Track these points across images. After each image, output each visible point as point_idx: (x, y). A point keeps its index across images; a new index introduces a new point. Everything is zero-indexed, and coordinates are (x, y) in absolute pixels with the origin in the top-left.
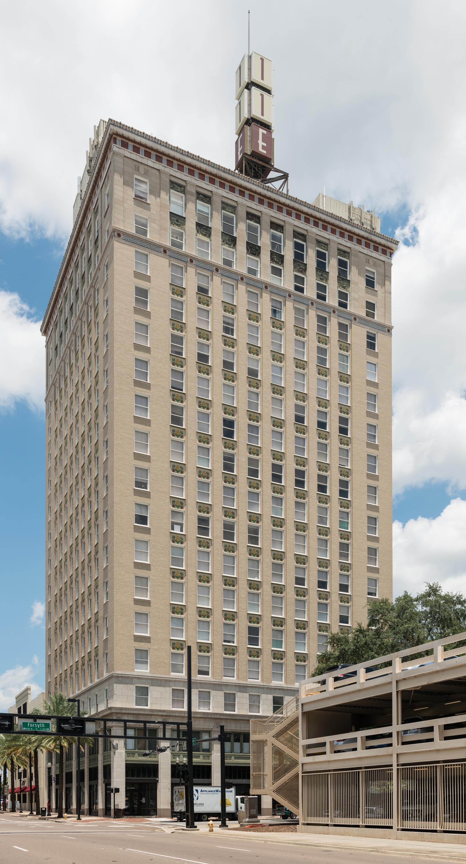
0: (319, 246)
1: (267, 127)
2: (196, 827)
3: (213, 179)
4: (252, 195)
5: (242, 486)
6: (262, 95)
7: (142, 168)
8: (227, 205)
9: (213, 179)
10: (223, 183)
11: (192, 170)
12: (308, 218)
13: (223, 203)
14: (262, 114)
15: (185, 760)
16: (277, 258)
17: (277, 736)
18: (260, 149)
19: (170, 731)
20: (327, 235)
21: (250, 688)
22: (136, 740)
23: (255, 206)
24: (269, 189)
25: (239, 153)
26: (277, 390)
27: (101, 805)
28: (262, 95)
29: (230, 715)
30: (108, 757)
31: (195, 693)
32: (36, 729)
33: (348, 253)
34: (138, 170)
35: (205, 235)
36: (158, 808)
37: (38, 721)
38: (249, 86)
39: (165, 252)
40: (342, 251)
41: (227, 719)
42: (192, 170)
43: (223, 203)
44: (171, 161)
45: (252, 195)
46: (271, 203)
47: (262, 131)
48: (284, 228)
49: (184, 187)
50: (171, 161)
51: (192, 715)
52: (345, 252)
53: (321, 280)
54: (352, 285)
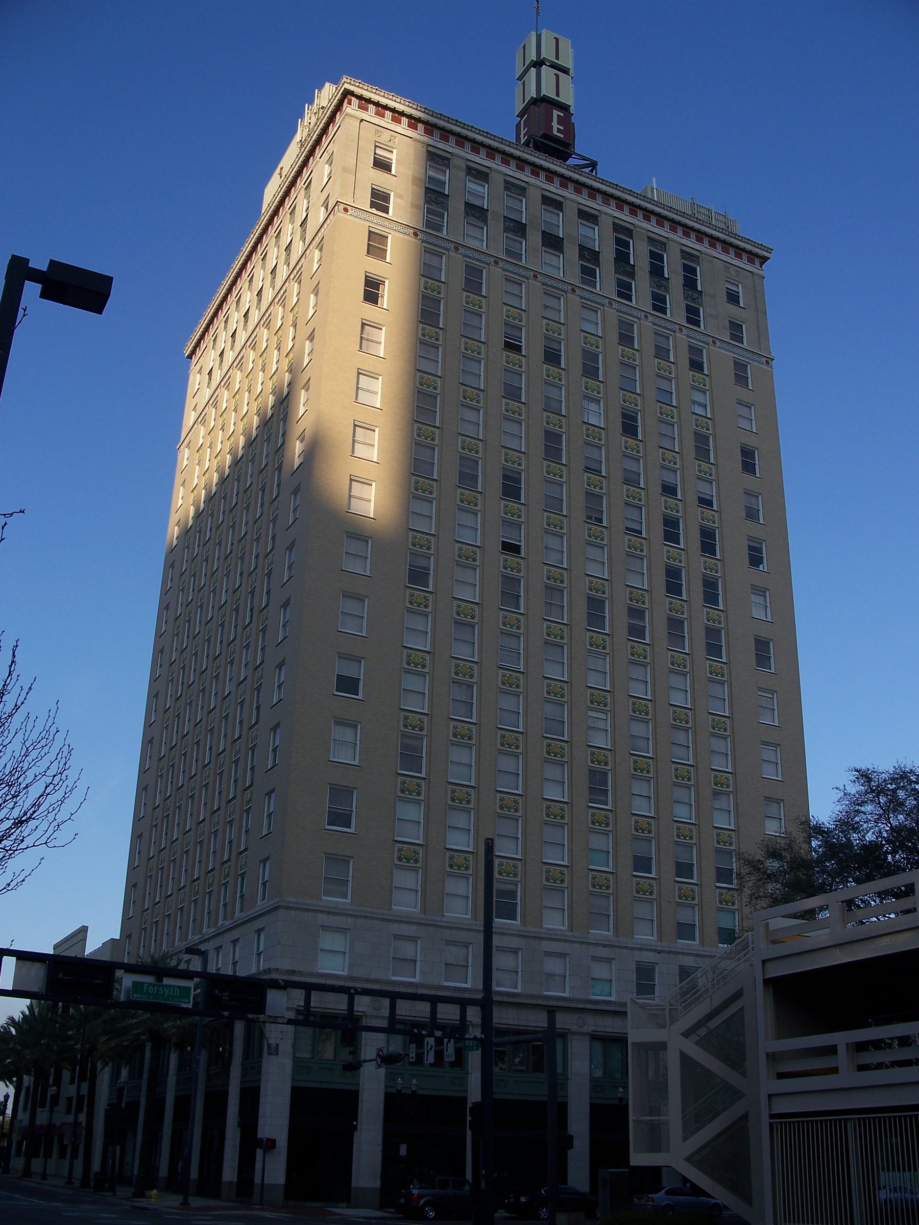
0: (652, 245)
1: (564, 108)
3: (492, 152)
4: (551, 175)
6: (557, 76)
9: (492, 152)
10: (507, 158)
11: (461, 140)
12: (634, 209)
14: (558, 95)
17: (686, 1034)
18: (555, 132)
20: (664, 232)
23: (554, 189)
25: (522, 136)
26: (593, 431)
27: (230, 1173)
28: (557, 76)
30: (253, 1067)
33: (698, 257)
35: (478, 218)
36: (353, 1185)
37: (167, 981)
38: (538, 64)
40: (688, 253)
42: (461, 140)
43: (505, 181)
45: (551, 175)
47: (556, 113)
48: (599, 219)
52: (692, 255)
53: (659, 287)
54: (705, 299)
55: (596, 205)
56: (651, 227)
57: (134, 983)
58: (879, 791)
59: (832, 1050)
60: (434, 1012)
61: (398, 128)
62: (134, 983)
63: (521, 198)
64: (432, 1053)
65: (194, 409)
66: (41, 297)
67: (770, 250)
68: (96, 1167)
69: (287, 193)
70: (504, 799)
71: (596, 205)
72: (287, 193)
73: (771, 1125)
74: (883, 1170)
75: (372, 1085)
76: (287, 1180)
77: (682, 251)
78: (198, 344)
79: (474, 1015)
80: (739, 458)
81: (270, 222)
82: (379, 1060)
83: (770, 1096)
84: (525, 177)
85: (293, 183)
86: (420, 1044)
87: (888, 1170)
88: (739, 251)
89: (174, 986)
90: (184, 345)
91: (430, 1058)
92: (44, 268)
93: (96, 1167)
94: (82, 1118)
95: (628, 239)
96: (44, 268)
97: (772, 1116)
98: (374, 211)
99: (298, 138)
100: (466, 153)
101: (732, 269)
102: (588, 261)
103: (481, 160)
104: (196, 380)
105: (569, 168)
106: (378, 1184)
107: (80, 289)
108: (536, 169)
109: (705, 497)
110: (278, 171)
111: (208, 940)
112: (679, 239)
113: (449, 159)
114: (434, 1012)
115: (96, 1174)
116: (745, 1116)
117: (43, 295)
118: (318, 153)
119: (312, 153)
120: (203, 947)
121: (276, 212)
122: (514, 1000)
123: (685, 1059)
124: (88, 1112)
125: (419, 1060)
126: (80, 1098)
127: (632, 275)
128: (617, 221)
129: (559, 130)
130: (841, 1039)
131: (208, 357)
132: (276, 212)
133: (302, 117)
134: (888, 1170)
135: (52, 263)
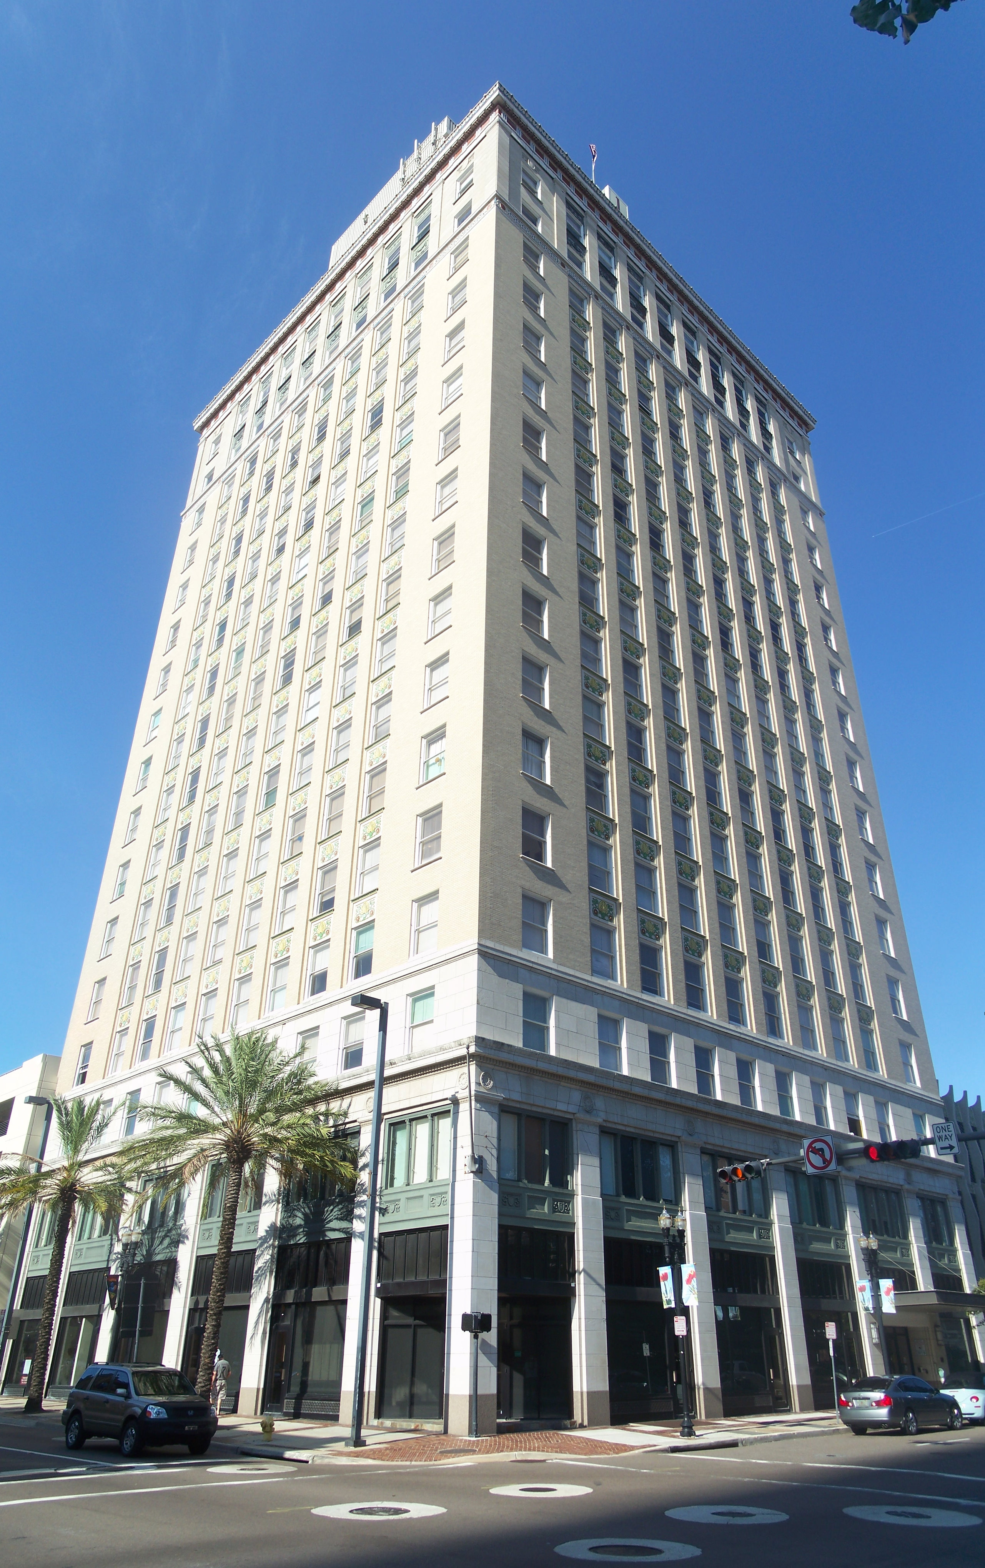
72: (361, 253)
106: (809, 1382)
110: (362, 216)
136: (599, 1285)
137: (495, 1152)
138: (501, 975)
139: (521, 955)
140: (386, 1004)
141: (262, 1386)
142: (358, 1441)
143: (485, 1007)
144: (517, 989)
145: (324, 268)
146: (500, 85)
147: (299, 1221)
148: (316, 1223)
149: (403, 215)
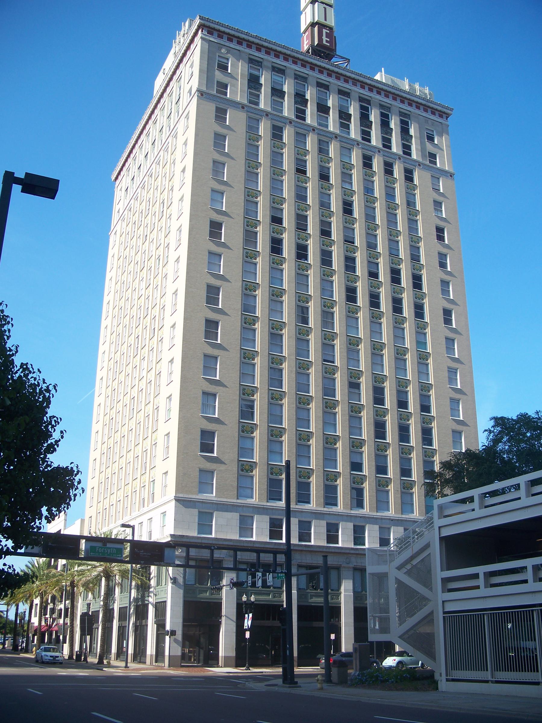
1: (331, 29)
2: (297, 683)
4: (321, 70)
5: (363, 317)
6: (325, 9)
7: (430, 121)
8: (300, 76)
11: (268, 51)
13: (295, 74)
15: (321, 600)
16: (344, 116)
17: (399, 568)
18: (324, 42)
19: (296, 567)
20: (389, 101)
21: (328, 516)
22: (198, 570)
23: (324, 78)
24: (332, 65)
28: (325, 9)
29: (306, 545)
31: (294, 522)
32: (106, 554)
33: (409, 115)
34: (428, 123)
39: (243, 108)
41: (301, 551)
42: (268, 51)
44: (250, 45)
45: (321, 70)
46: (338, 76)
49: (261, 62)
50: (250, 45)
51: (292, 548)
52: (406, 114)
53: (386, 134)
55: (348, 86)
56: (381, 98)
57: (91, 546)
58: (512, 429)
59: (476, 576)
60: (258, 557)
61: (232, 45)
62: (91, 546)
63: (304, 83)
64: (260, 581)
65: (118, 212)
66: (22, 192)
67: (452, 110)
68: (77, 648)
69: (168, 85)
70: (301, 434)
71: (348, 86)
72: (168, 85)
73: (444, 617)
74: (523, 641)
75: (228, 598)
76: (237, 653)
77: (400, 112)
78: (119, 174)
79: (281, 558)
80: (435, 233)
81: (158, 101)
82: (231, 585)
83: (443, 602)
84: (307, 71)
85: (171, 79)
86: (254, 576)
87: (526, 641)
88: (434, 111)
89: (113, 548)
90: (111, 174)
91: (259, 583)
92: (22, 176)
93: (77, 648)
94: (68, 621)
95: (368, 106)
96: (22, 176)
97: (445, 613)
98: (219, 95)
99: (172, 51)
100: (271, 59)
101: (430, 121)
102: (345, 120)
103: (280, 62)
104: (119, 194)
105: (332, 65)
106: (234, 654)
107: (43, 187)
108: (313, 67)
109: (374, 293)
110: (162, 71)
111: (135, 518)
112: (398, 105)
113: (261, 62)
114: (258, 557)
115: (77, 652)
116: (432, 612)
117: (23, 191)
118: (185, 60)
119: (181, 61)
120: (131, 524)
121: (162, 96)
122: (309, 549)
123: (399, 582)
124: (70, 617)
125: (254, 584)
126: (66, 610)
127: (370, 127)
128: (361, 95)
129: (327, 41)
130: (481, 570)
131: (124, 181)
132: (162, 96)
133: (175, 39)
134: (526, 641)
135: (27, 174)
136: (232, 620)
137: (182, 575)
138: (186, 507)
139: (197, 497)
140: (134, 526)
141: (154, 653)
142: (126, 666)
143: (177, 522)
144: (195, 512)
145: (151, 96)
146: (200, 16)
147: (140, 597)
148: (143, 597)
149: (196, 39)
